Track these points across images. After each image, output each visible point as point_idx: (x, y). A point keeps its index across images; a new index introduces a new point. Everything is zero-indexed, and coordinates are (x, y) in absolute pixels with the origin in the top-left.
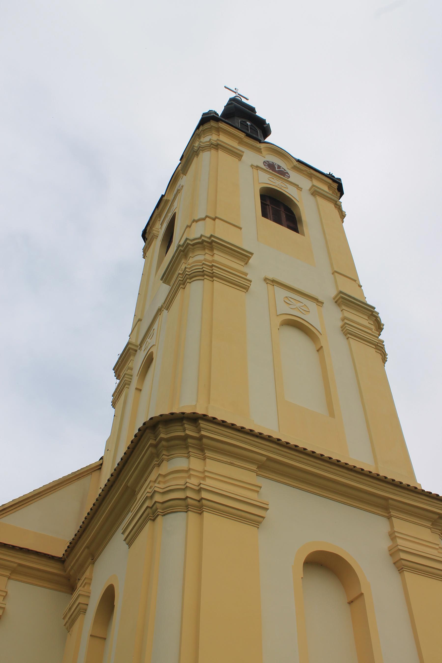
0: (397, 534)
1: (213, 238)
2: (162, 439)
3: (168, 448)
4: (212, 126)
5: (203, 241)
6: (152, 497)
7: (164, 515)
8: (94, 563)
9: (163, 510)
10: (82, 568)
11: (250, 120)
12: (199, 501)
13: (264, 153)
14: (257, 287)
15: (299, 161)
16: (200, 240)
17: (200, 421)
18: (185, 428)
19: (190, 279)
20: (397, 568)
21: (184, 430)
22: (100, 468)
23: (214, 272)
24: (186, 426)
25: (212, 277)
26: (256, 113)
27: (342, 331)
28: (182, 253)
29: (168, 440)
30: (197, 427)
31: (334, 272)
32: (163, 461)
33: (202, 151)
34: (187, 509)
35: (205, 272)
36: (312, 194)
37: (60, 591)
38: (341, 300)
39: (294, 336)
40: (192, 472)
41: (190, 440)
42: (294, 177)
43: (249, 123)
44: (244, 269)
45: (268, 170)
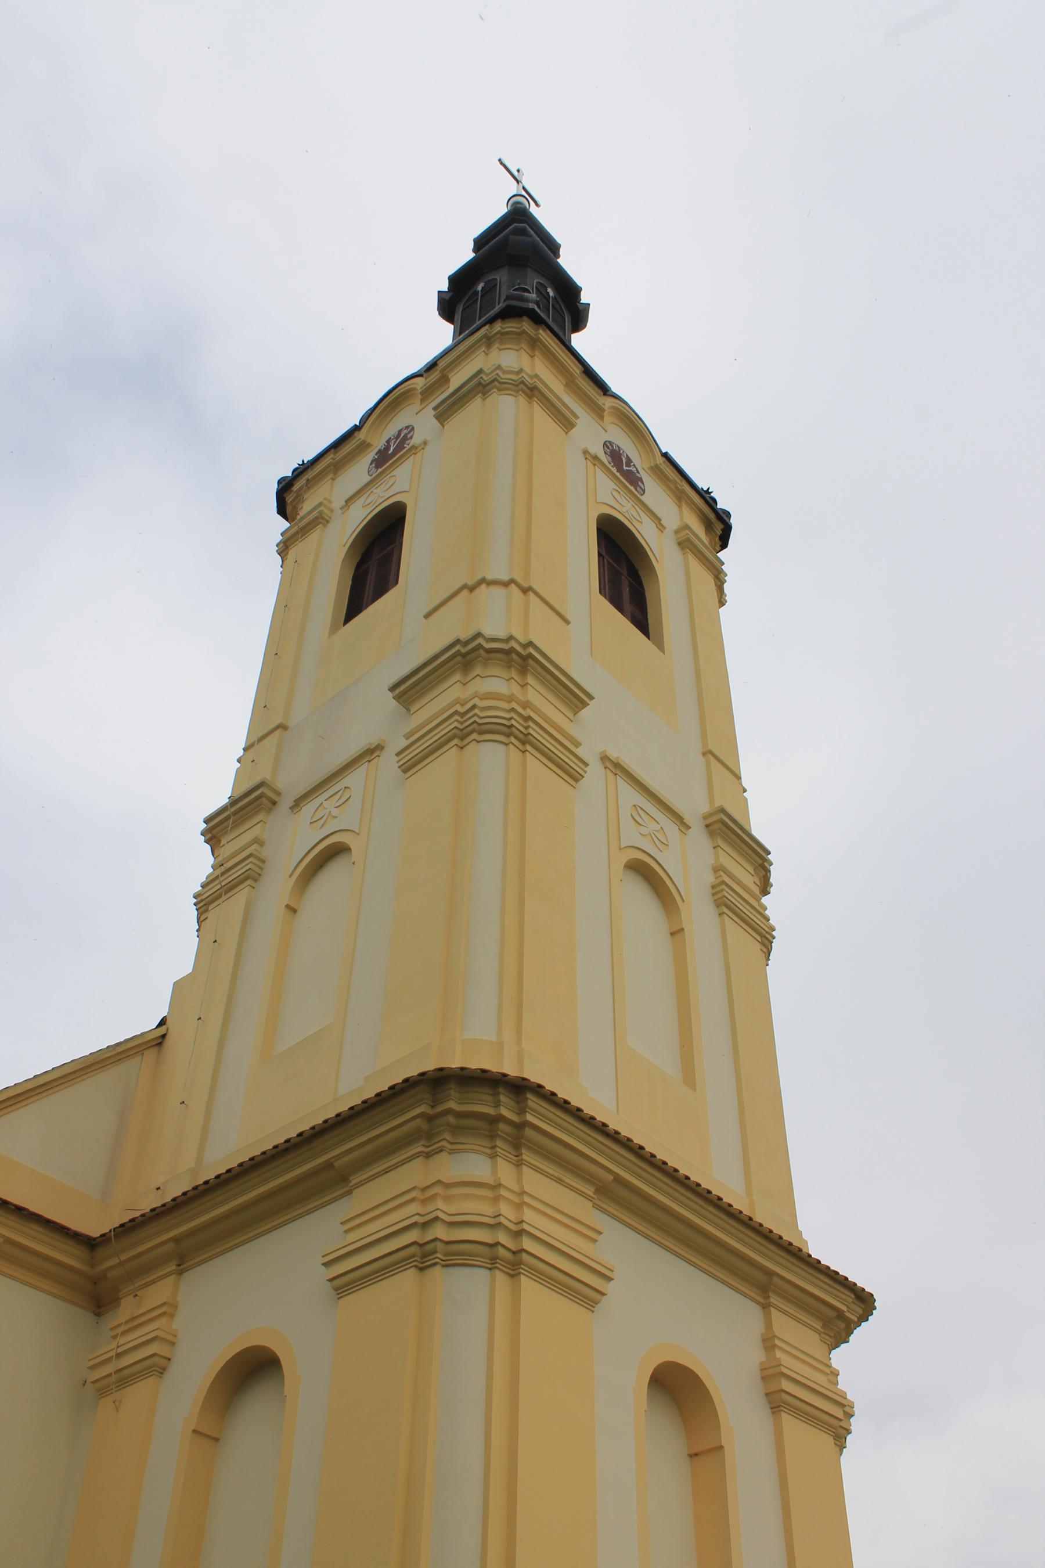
0: (777, 1342)
1: (531, 650)
2: (449, 1111)
3: (455, 1130)
4: (524, 332)
5: (512, 650)
6: (425, 1226)
8: (181, 1273)
9: (446, 1255)
10: (142, 1271)
11: (556, 289)
12: (514, 1253)
13: (608, 418)
14: (595, 775)
15: (666, 455)
16: (505, 646)
17: (529, 1095)
18: (499, 1101)
19: (481, 733)
20: (770, 1403)
21: (497, 1104)
22: (160, 1044)
24: (503, 1098)
25: (524, 743)
26: (558, 256)
27: (713, 895)
28: (459, 658)
29: (459, 1115)
30: (518, 1102)
31: (707, 753)
32: (441, 1151)
33: (499, 390)
34: (492, 1263)
35: (514, 729)
36: (679, 544)
37: (72, 1302)
38: (719, 825)
39: (638, 898)
40: (503, 1192)
41: (502, 1126)
42: (655, 494)
43: (551, 292)
45: (609, 466)
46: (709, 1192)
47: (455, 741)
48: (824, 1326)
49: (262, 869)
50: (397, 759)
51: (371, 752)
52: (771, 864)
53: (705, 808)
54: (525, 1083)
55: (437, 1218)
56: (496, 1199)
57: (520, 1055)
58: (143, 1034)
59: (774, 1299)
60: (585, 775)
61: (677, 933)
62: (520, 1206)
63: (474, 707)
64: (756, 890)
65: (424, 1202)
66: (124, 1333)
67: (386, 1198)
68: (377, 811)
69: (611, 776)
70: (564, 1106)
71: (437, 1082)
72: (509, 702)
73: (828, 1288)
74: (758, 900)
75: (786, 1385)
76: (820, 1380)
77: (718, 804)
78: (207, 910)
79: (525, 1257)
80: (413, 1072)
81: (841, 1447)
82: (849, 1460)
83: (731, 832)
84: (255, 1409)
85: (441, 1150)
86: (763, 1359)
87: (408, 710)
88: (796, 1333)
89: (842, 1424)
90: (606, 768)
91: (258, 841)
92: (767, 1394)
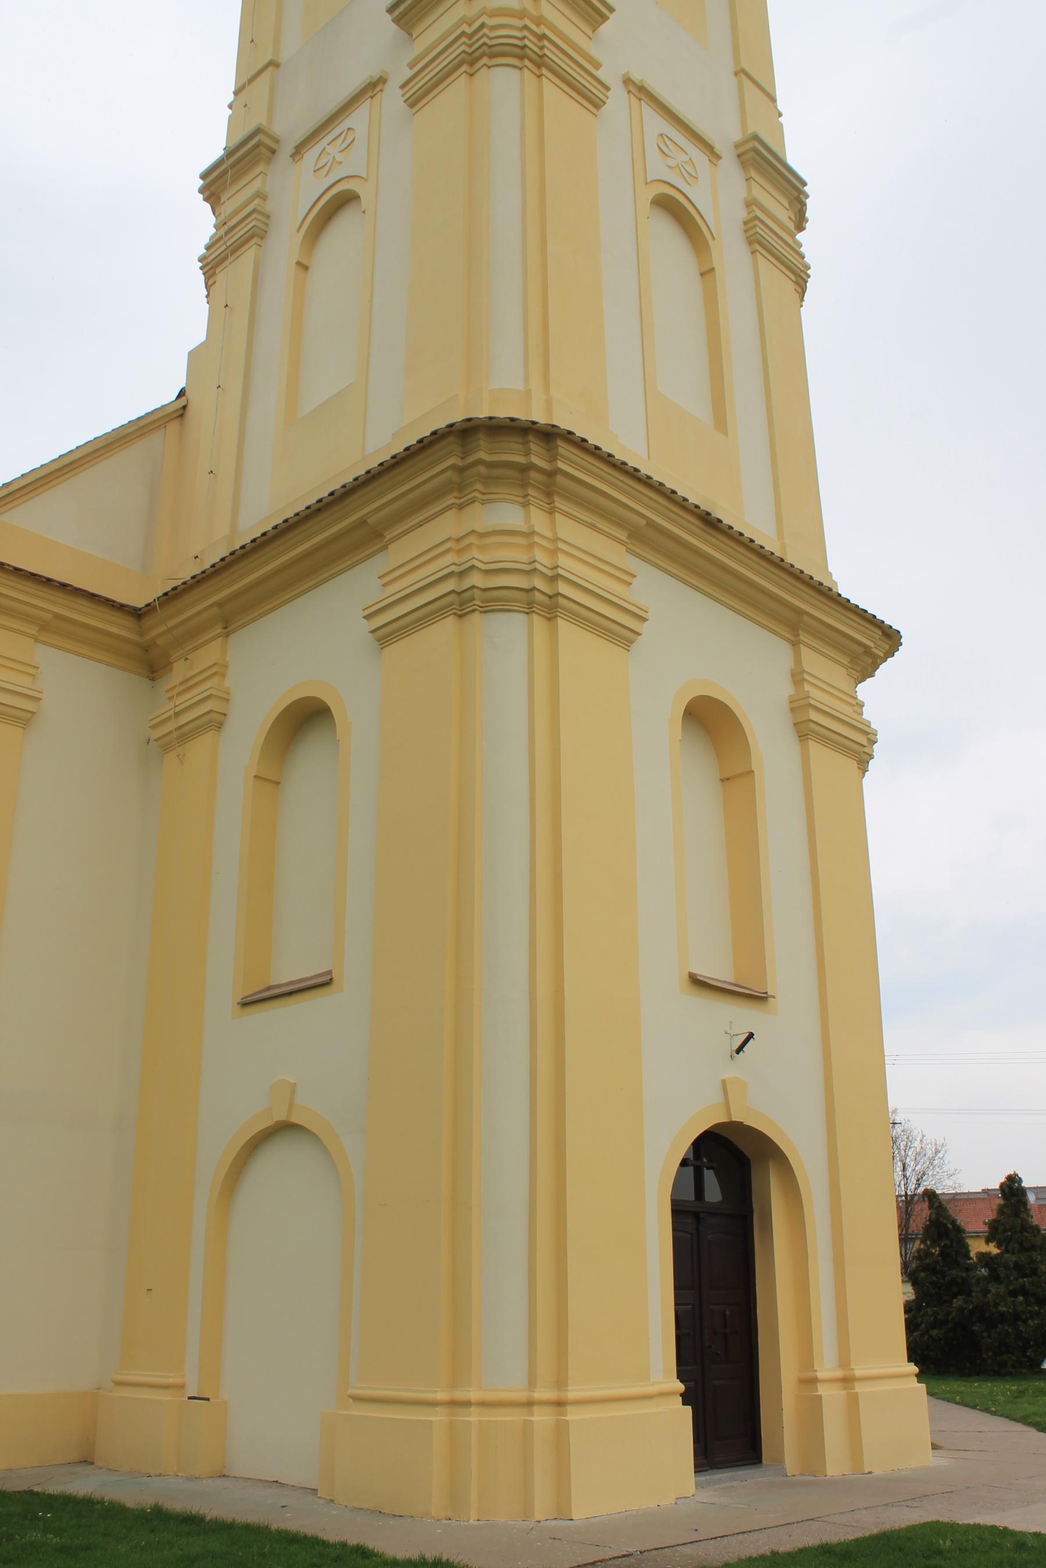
0: (806, 676)
2: (479, 462)
3: (487, 480)
6: (462, 574)
7: (486, 612)
8: (227, 635)
9: (483, 602)
10: (191, 636)
12: (550, 597)
14: (617, 100)
17: (559, 442)
19: (491, 56)
20: (798, 732)
21: (527, 453)
22: (182, 415)
23: (545, 55)
24: (532, 446)
27: (745, 231)
29: (490, 465)
30: (548, 450)
32: (474, 501)
34: (530, 608)
38: (751, 154)
39: (665, 233)
40: (537, 539)
44: (592, 49)
46: (741, 534)
47: (464, 68)
48: (851, 662)
49: (267, 225)
50: (402, 92)
51: (373, 87)
52: (807, 197)
53: (737, 136)
54: (555, 430)
55: (473, 567)
56: (531, 546)
57: (549, 402)
58: (163, 407)
59: (803, 637)
60: (607, 101)
61: (707, 273)
62: (554, 552)
63: (483, 26)
64: (791, 226)
65: (459, 552)
66: (179, 694)
67: (423, 550)
68: (385, 151)
69: (634, 102)
70: (595, 452)
71: (466, 432)
72: (521, 19)
73: (857, 626)
74: (793, 236)
75: (814, 716)
76: (847, 710)
77: (750, 131)
78: (214, 274)
79: (561, 600)
80: (441, 424)
81: (864, 770)
82: (868, 781)
83: (763, 161)
84: (311, 757)
85: (473, 501)
86: (792, 692)
87: (410, 34)
88: (824, 668)
89: (866, 750)
90: (629, 92)
91: (261, 196)
92: (795, 724)
